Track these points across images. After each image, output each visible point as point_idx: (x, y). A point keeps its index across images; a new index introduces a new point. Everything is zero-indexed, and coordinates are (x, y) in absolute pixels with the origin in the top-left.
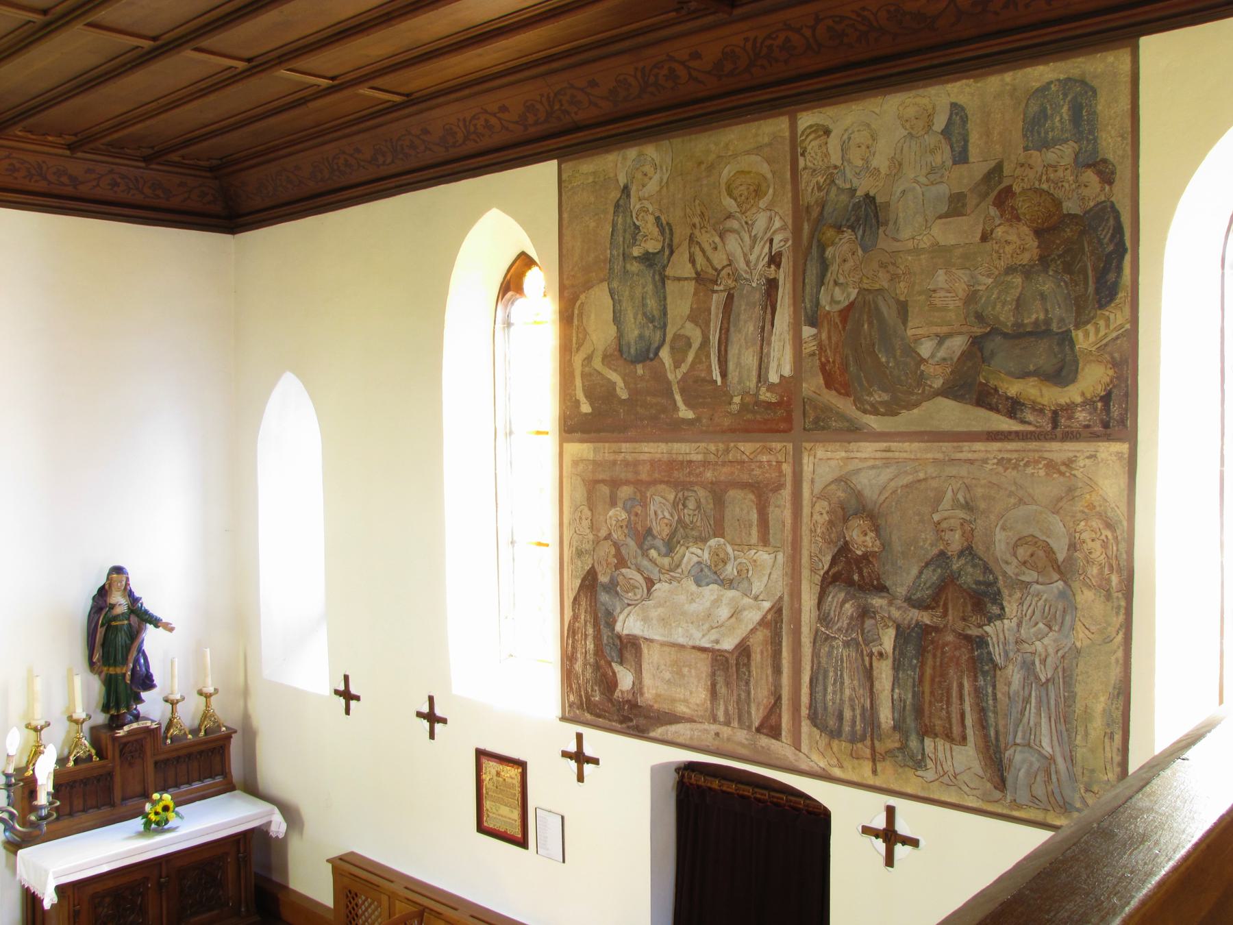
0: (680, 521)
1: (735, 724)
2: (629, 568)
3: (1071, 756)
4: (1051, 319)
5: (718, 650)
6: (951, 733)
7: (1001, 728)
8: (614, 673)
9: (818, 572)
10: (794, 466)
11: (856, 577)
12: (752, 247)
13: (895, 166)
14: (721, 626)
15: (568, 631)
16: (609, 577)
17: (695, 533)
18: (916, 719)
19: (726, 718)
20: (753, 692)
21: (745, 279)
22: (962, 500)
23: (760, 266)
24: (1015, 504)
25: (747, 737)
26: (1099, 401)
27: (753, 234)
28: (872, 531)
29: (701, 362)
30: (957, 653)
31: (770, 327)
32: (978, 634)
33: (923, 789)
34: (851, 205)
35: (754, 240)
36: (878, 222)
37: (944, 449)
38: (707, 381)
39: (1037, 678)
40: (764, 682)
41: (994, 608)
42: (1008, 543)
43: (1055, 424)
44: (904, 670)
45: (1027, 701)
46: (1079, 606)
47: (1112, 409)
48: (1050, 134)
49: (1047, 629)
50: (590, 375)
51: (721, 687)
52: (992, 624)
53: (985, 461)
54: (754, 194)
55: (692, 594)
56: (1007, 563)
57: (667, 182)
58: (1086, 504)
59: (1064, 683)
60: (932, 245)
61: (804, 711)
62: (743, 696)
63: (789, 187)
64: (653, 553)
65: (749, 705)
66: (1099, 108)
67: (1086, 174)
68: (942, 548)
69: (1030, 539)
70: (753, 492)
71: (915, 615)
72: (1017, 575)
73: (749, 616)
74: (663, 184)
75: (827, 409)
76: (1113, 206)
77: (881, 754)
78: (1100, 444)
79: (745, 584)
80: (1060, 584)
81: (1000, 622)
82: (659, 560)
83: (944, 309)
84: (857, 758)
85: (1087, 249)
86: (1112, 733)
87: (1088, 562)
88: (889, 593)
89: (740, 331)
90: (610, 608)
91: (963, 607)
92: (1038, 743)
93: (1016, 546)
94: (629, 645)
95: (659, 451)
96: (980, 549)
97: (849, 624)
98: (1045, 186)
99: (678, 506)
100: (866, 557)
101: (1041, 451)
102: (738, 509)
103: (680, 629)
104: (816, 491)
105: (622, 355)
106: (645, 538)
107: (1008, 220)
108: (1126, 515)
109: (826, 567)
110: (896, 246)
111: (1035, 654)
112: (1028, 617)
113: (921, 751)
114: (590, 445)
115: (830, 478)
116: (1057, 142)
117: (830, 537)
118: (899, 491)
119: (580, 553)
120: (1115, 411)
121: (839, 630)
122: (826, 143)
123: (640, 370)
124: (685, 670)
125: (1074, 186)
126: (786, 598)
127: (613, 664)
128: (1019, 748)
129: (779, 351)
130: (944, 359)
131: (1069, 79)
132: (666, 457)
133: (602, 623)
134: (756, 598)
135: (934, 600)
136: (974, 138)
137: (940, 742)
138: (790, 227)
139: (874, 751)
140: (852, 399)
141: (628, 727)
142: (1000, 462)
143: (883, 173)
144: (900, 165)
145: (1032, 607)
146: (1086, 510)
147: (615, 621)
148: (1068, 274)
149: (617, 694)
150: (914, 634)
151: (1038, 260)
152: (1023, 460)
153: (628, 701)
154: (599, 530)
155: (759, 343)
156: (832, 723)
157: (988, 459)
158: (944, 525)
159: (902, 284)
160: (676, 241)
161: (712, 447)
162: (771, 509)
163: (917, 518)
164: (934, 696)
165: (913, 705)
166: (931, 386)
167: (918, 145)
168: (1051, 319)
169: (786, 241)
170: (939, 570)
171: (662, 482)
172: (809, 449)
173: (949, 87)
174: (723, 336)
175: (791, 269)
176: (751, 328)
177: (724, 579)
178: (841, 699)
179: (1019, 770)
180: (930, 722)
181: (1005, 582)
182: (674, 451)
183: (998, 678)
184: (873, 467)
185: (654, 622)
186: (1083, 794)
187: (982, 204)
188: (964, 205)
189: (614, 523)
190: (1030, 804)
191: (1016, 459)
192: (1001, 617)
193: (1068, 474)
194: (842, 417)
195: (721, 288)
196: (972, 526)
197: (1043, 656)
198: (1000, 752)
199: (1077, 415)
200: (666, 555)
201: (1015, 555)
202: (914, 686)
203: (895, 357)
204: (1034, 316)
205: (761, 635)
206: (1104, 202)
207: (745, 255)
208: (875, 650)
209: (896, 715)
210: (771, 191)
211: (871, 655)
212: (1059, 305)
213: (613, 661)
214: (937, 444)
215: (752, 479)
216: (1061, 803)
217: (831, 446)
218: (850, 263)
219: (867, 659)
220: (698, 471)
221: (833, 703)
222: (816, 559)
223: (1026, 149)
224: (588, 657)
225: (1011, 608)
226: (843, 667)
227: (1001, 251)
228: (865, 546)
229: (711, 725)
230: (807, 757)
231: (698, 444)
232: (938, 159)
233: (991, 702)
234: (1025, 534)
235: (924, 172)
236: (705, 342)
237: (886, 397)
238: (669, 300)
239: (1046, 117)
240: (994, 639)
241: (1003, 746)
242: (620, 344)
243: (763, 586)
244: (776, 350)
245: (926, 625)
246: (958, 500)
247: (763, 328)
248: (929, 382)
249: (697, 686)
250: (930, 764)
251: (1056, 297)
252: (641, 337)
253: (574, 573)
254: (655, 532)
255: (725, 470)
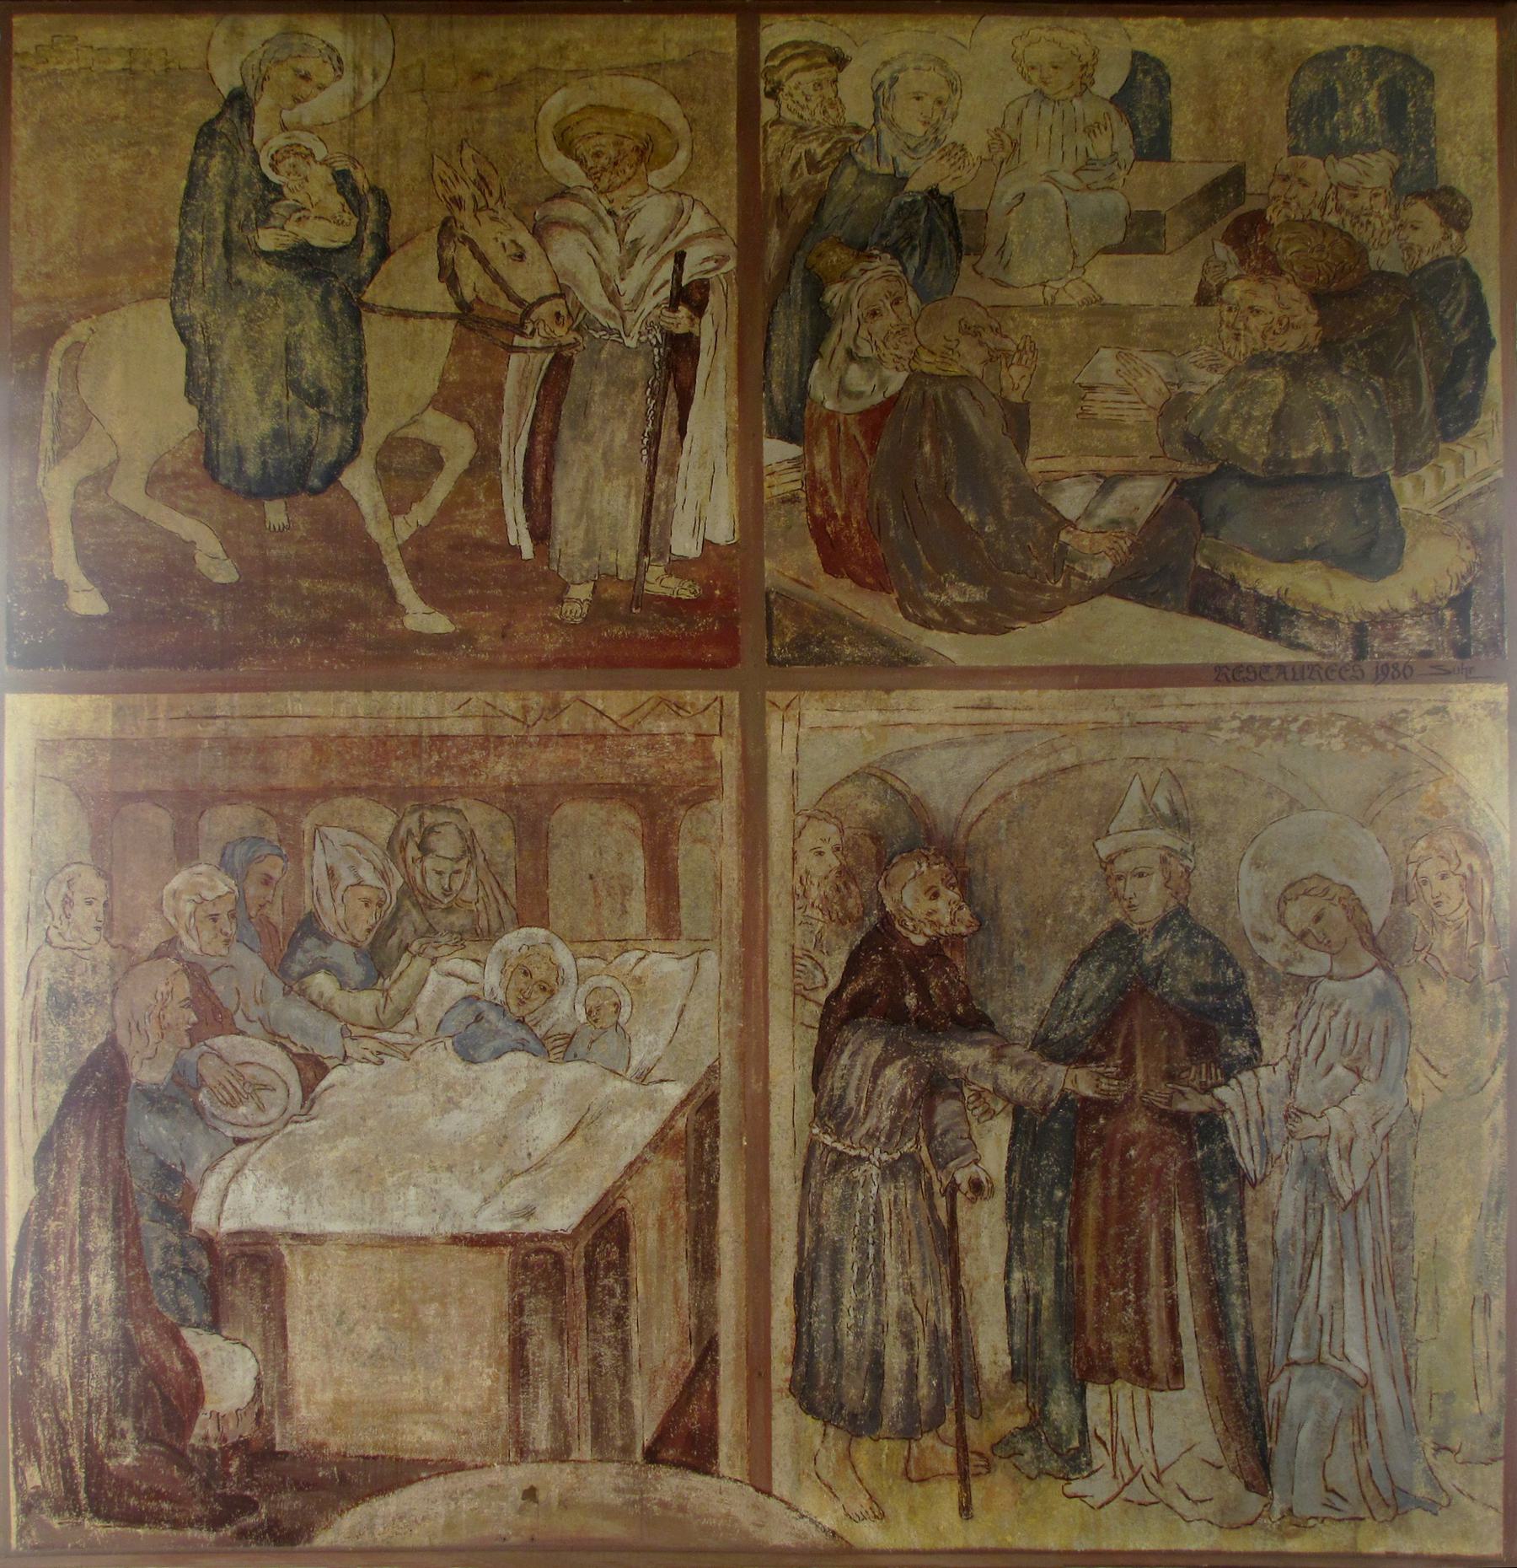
0: (410, 890)
1: (584, 1449)
2: (241, 1033)
3: (1407, 1369)
4: (1348, 454)
5: (533, 1237)
6: (1149, 1362)
7: (1258, 1328)
8: (190, 1363)
9: (812, 995)
10: (744, 746)
11: (911, 1000)
12: (626, 265)
13: (1003, 146)
14: (539, 1167)
15: (21, 1247)
16: (169, 1066)
17: (458, 920)
18: (1066, 1341)
19: (555, 1439)
20: (636, 1342)
21: (603, 328)
22: (1165, 809)
23: (648, 305)
24: (1280, 812)
25: (620, 1482)
26: (1447, 607)
27: (629, 237)
28: (950, 886)
29: (470, 503)
30: (1156, 1161)
31: (674, 435)
32: (1203, 1108)
33: (1084, 1527)
34: (892, 206)
35: (634, 249)
36: (959, 247)
37: (1119, 702)
38: (489, 547)
39: (1334, 1193)
40: (667, 1306)
41: (1237, 1043)
42: (1266, 897)
43: (1360, 647)
44: (1034, 1219)
45: (1312, 1251)
46: (1416, 1020)
47: (1473, 623)
48: (1343, 135)
49: (1352, 1077)
50: (105, 520)
51: (541, 1345)
52: (1233, 1082)
53: (1214, 724)
54: (634, 157)
55: (448, 1086)
56: (1265, 939)
57: (375, 102)
58: (1429, 805)
59: (1389, 1195)
60: (1087, 302)
61: (781, 1373)
62: (608, 1356)
63: (731, 154)
64: (322, 983)
65: (624, 1382)
66: (1439, 104)
67: (1415, 208)
68: (1118, 915)
69: (1313, 883)
70: (632, 806)
71: (1060, 1078)
72: (1288, 963)
73: (623, 1129)
74: (361, 104)
75: (830, 617)
76: (1466, 266)
77: (980, 1455)
78: (1452, 686)
79: (612, 1041)
80: (1378, 973)
81: (1250, 1074)
82: (342, 1001)
83: (1114, 424)
84: (922, 1480)
85: (1417, 335)
86: (1487, 1297)
87: (1433, 924)
88: (994, 1032)
89: (588, 440)
90: (173, 1161)
91: (1169, 1047)
92: (1337, 1351)
93: (1283, 900)
94: (240, 1264)
95: (342, 711)
96: (1204, 910)
97: (894, 1120)
98: (1333, 219)
99: (403, 849)
100: (935, 949)
101: (1333, 702)
102: (588, 852)
103: (412, 1192)
104: (803, 802)
105: (215, 479)
106: (294, 943)
107: (1254, 271)
108: (1507, 821)
109: (833, 983)
110: (1001, 295)
111: (1328, 1137)
112: (1311, 1056)
113: (1077, 1424)
114: (106, 701)
115: (840, 771)
116: (1353, 148)
117: (843, 907)
118: (1015, 793)
119: (62, 1003)
120: (1479, 627)
121: (870, 1136)
122: (835, 81)
123: (276, 513)
124: (429, 1313)
125: (1391, 225)
126: (728, 1069)
127: (187, 1334)
128: (1298, 1372)
129: (698, 487)
130: (1115, 523)
131: (1378, 50)
132: (364, 727)
133: (147, 1208)
134: (642, 1078)
135: (1100, 1038)
136: (1184, 119)
137: (1123, 1389)
138: (733, 232)
139: (965, 1449)
140: (894, 596)
141: (242, 1534)
142: (1247, 725)
143: (975, 155)
144: (1015, 144)
145: (1319, 1033)
146: (1429, 817)
147: (191, 1197)
148: (1380, 375)
149: (203, 1430)
150: (1056, 1126)
151: (1320, 347)
152: (1296, 720)
153: (241, 1446)
154: (133, 933)
155: (643, 468)
156: (854, 1392)
157: (1219, 720)
158: (1123, 865)
159: (1014, 370)
160: (398, 230)
161: (509, 702)
162: (683, 847)
163: (1059, 852)
164: (1107, 1275)
165: (1057, 1304)
166: (1083, 576)
167: (1058, 114)
168: (1348, 454)
169: (721, 260)
170: (1113, 968)
171: (349, 790)
172: (783, 705)
173: (1130, 23)
174: (539, 448)
175: (734, 319)
176: (622, 435)
177: (546, 1037)
178: (877, 1322)
179: (1300, 1427)
180: (1100, 1341)
181: (1260, 982)
182: (393, 713)
183: (1248, 1209)
184: (950, 743)
185: (326, 1181)
186: (1432, 1460)
187: (1200, 237)
188: (1159, 235)
189: (189, 908)
190: (1326, 1512)
191: (1284, 720)
192: (1251, 1063)
193: (1390, 746)
194: (869, 634)
195: (537, 342)
196: (1186, 862)
197: (1345, 1141)
198: (1258, 1391)
199: (1404, 633)
200: (365, 985)
201: (1281, 920)
202: (1059, 1256)
203: (997, 513)
204: (1311, 448)
205: (663, 1173)
206: (1448, 258)
207: (605, 280)
208: (962, 1177)
209: (1017, 1339)
210: (682, 155)
211: (952, 1191)
212: (1362, 428)
213: (185, 1321)
214: (1104, 691)
215: (629, 775)
216: (1387, 1495)
217: (841, 699)
218: (889, 320)
219: (941, 1203)
220: (465, 759)
221: (859, 1335)
222: (808, 963)
223: (1294, 151)
224: (94, 1325)
225: (1274, 1038)
226: (880, 1233)
227: (1241, 326)
228: (933, 923)
229: (512, 1469)
230: (789, 1506)
231: (465, 695)
232: (1101, 146)
233: (1234, 1268)
234: (1304, 874)
235: (1070, 163)
236: (486, 458)
237: (976, 594)
238: (373, 358)
239: (1334, 105)
240: (1239, 1117)
241: (1262, 1372)
242: (208, 449)
243: (662, 1043)
244: (691, 484)
245: (1085, 1099)
246: (1156, 808)
247: (655, 437)
248: (1078, 568)
249: (467, 1355)
250: (1100, 1455)
251: (1356, 415)
252: (280, 437)
253: (42, 1062)
254: (328, 924)
255: (551, 755)
